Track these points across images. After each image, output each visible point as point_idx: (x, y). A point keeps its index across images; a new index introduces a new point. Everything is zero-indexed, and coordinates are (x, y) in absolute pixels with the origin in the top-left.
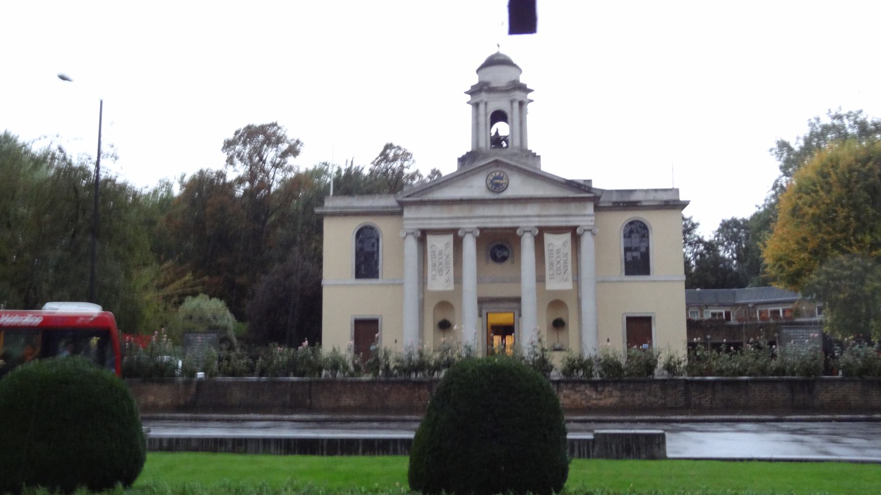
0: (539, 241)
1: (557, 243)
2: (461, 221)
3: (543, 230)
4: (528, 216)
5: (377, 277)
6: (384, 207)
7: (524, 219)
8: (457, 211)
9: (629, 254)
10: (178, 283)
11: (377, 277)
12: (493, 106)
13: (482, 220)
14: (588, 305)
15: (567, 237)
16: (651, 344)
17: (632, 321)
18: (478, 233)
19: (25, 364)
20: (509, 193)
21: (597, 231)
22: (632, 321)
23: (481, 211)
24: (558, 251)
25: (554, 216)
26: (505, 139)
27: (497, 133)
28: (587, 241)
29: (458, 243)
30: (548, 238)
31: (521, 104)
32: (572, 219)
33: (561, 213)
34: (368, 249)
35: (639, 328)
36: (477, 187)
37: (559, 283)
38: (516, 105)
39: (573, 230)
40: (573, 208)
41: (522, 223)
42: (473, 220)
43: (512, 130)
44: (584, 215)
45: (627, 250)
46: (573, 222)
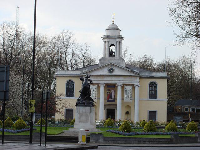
0: (123, 88)
1: (128, 88)
2: (100, 81)
3: (124, 85)
4: (120, 81)
5: (156, 98)
6: (75, 75)
7: (118, 82)
8: (99, 78)
9: (151, 92)
10: (46, 98)
11: (156, 98)
12: (110, 43)
13: (106, 81)
14: (136, 108)
15: (131, 87)
16: (156, 120)
17: (150, 112)
18: (105, 85)
19: (57, 107)
20: (114, 74)
21: (140, 86)
22: (150, 112)
23: (106, 79)
24: (128, 91)
25: (127, 81)
26: (114, 53)
27: (112, 51)
28: (137, 88)
29: (99, 87)
30: (126, 87)
31: (120, 42)
32: (132, 82)
33: (129, 80)
34: (70, 87)
35: (152, 114)
36: (105, 72)
37: (128, 100)
38: (118, 43)
39: (133, 85)
40: (133, 79)
41: (118, 83)
42: (104, 81)
43: (116, 48)
44: (136, 81)
45: (150, 90)
46: (133, 83)
